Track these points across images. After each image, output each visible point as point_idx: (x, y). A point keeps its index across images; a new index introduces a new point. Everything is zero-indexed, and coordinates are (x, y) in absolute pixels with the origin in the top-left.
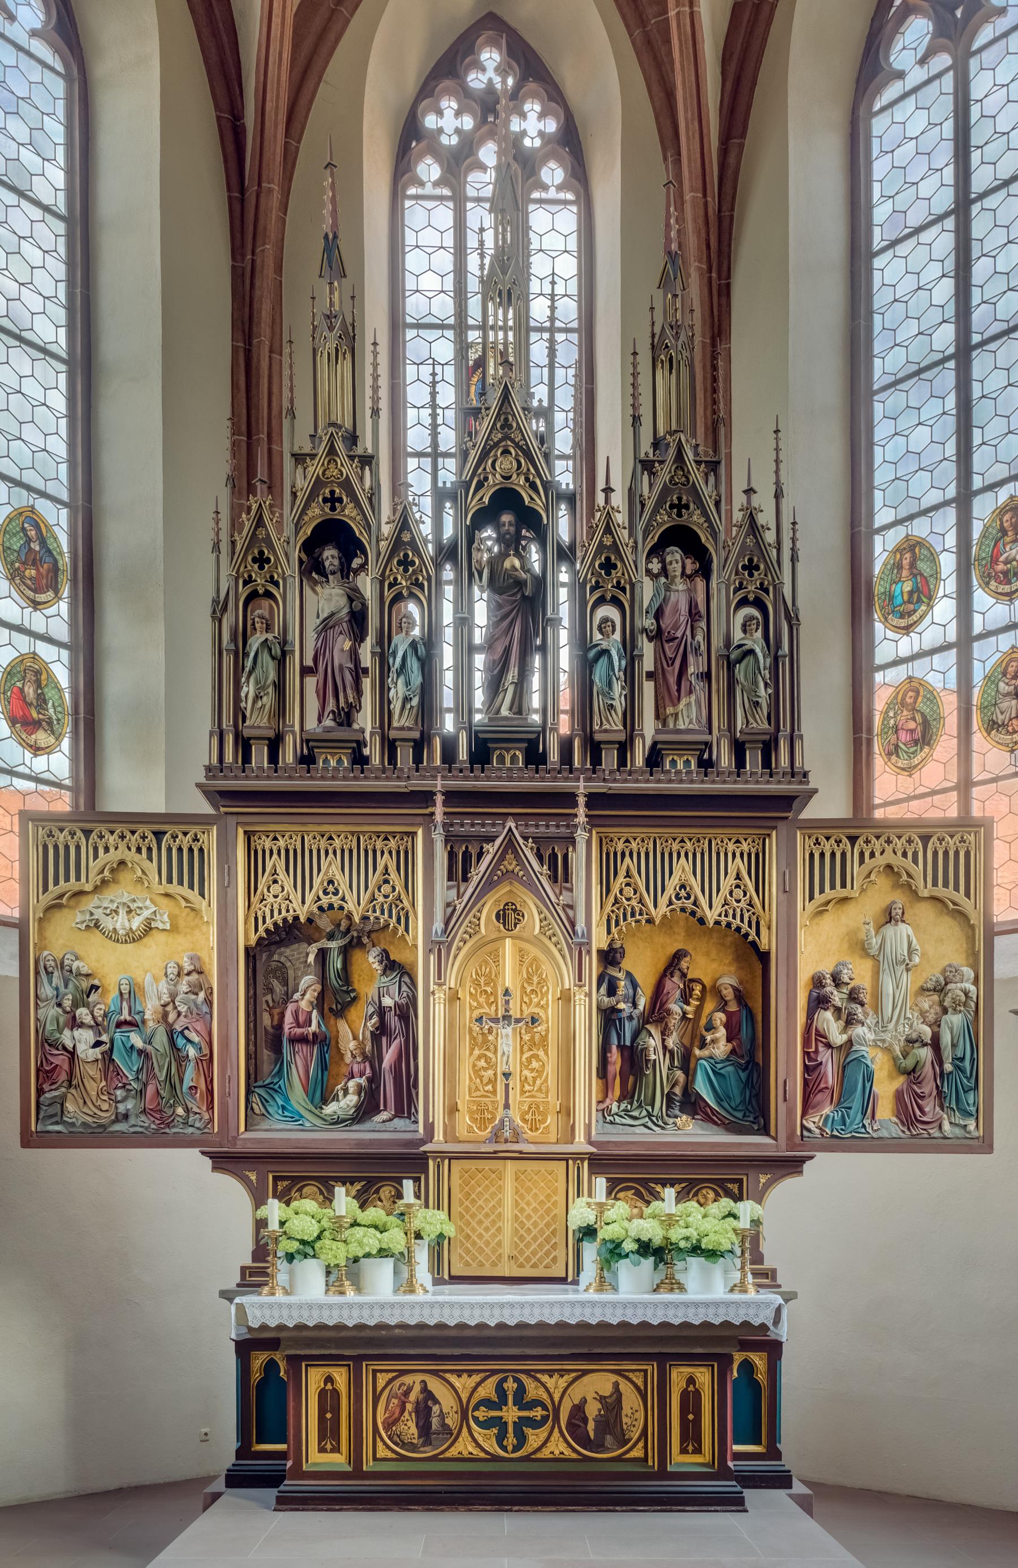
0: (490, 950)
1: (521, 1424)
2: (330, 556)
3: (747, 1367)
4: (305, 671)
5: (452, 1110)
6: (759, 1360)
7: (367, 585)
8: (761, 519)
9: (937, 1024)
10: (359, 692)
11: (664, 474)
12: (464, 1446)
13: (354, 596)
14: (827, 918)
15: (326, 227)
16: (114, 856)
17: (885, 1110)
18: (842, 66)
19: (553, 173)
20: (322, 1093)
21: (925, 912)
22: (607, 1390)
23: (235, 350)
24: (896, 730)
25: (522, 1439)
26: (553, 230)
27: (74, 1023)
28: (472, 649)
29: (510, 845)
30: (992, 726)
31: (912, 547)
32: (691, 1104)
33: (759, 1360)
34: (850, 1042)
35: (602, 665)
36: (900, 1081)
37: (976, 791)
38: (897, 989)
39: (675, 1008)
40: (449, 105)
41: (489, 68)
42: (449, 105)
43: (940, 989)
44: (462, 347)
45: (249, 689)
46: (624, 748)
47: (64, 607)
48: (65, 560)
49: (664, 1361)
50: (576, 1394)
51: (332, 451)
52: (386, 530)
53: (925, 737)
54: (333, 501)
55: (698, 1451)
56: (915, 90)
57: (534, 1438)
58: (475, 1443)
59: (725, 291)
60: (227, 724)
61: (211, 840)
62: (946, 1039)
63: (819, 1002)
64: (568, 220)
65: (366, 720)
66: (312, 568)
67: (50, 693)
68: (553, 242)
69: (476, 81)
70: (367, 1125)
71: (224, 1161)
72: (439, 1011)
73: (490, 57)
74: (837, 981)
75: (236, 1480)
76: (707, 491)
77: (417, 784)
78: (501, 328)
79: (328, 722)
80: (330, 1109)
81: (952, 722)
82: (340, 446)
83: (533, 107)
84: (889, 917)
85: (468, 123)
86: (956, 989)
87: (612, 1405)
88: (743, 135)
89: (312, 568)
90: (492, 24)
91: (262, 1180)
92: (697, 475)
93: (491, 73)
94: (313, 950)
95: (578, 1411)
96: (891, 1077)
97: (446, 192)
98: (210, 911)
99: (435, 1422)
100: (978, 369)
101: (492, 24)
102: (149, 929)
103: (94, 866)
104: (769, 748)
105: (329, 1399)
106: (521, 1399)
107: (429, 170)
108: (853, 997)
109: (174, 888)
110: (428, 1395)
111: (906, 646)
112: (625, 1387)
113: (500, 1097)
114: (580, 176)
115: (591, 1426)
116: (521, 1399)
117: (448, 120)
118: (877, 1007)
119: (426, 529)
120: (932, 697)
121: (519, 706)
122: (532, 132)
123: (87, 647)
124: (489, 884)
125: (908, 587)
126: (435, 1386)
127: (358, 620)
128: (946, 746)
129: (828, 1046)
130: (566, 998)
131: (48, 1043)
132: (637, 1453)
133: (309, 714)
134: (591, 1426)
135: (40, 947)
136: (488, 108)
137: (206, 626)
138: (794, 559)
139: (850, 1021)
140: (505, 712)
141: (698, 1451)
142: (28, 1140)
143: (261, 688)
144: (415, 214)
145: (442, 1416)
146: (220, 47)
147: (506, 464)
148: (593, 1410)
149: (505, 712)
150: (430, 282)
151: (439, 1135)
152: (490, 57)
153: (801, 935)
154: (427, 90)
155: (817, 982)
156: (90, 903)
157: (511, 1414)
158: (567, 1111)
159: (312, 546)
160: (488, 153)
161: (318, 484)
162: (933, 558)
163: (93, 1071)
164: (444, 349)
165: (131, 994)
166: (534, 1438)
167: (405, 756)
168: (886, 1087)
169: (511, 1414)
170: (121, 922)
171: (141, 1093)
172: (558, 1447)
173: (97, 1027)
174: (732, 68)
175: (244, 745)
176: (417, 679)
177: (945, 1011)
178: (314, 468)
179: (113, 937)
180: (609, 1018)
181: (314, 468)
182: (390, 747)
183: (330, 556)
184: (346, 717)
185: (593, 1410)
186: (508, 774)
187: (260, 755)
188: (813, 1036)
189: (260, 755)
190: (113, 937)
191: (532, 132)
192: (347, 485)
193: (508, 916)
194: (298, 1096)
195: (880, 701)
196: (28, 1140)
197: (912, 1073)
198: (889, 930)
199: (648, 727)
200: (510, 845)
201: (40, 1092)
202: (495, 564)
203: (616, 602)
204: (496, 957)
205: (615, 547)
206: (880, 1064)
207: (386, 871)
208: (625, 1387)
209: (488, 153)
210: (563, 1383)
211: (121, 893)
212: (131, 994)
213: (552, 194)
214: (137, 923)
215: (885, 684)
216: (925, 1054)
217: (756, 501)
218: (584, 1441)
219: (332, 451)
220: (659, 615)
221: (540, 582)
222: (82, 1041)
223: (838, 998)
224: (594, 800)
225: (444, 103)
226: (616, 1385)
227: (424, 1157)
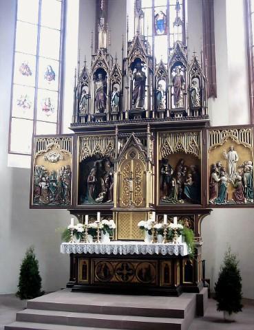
1: (128, 274)
4: (172, 95)
5: (118, 200)
8: (197, 59)
9: (242, 176)
10: (105, 104)
12: (114, 279)
14: (215, 151)
16: (52, 144)
17: (230, 198)
20: (95, 195)
21: (240, 148)
22: (147, 266)
25: (127, 278)
27: (42, 181)
32: (182, 196)
34: (221, 181)
36: (234, 190)
38: (233, 167)
39: (179, 173)
43: (244, 167)
50: (140, 267)
55: (168, 282)
57: (130, 278)
58: (116, 278)
60: (76, 114)
61: (72, 139)
62: (245, 179)
63: (213, 171)
65: (107, 111)
66: (96, 79)
70: (105, 203)
71: (72, 212)
74: (217, 166)
75: (68, 286)
76: (185, 54)
79: (97, 112)
80: (98, 199)
84: (230, 150)
86: (247, 167)
87: (148, 270)
89: (96, 79)
92: (182, 50)
94: (95, 163)
95: (140, 272)
96: (232, 189)
98: (71, 155)
99: (108, 273)
102: (58, 160)
103: (47, 146)
104: (200, 110)
105: (84, 267)
106: (128, 269)
108: (222, 170)
109: (64, 150)
110: (106, 267)
112: (152, 266)
115: (143, 276)
116: (128, 269)
118: (228, 171)
121: (141, 104)
126: (108, 264)
127: (105, 89)
129: (215, 181)
131: (36, 185)
132: (154, 282)
133: (93, 111)
134: (143, 276)
135: (36, 164)
137: (73, 93)
139: (221, 176)
140: (137, 107)
141: (168, 282)
142: (31, 207)
143: (84, 106)
145: (109, 272)
148: (144, 271)
151: (115, 206)
153: (208, 155)
155: (213, 166)
156: (46, 154)
157: (125, 272)
159: (96, 74)
163: (46, 192)
165: (55, 173)
166: (130, 278)
167: (114, 118)
168: (230, 191)
169: (125, 272)
170: (52, 158)
171: (55, 196)
172: (135, 280)
173: (47, 182)
175: (79, 118)
177: (245, 172)
178: (96, 58)
179: (51, 161)
180: (163, 176)
181: (96, 58)
182: (111, 116)
184: (102, 111)
185: (144, 271)
186: (138, 122)
187: (83, 120)
188: (212, 179)
189: (83, 120)
190: (51, 161)
192: (103, 61)
193: (132, 155)
194: (90, 197)
196: (31, 207)
197: (237, 188)
198: (230, 153)
201: (34, 196)
202: (135, 74)
203: (197, 77)
204: (130, 164)
206: (228, 185)
207: (110, 144)
210: (137, 264)
211: (52, 152)
212: (55, 173)
214: (56, 158)
216: (240, 182)
217: (196, 55)
218: (141, 278)
222: (43, 185)
223: (217, 170)
224: (151, 126)
226: (149, 266)
227: (112, 211)
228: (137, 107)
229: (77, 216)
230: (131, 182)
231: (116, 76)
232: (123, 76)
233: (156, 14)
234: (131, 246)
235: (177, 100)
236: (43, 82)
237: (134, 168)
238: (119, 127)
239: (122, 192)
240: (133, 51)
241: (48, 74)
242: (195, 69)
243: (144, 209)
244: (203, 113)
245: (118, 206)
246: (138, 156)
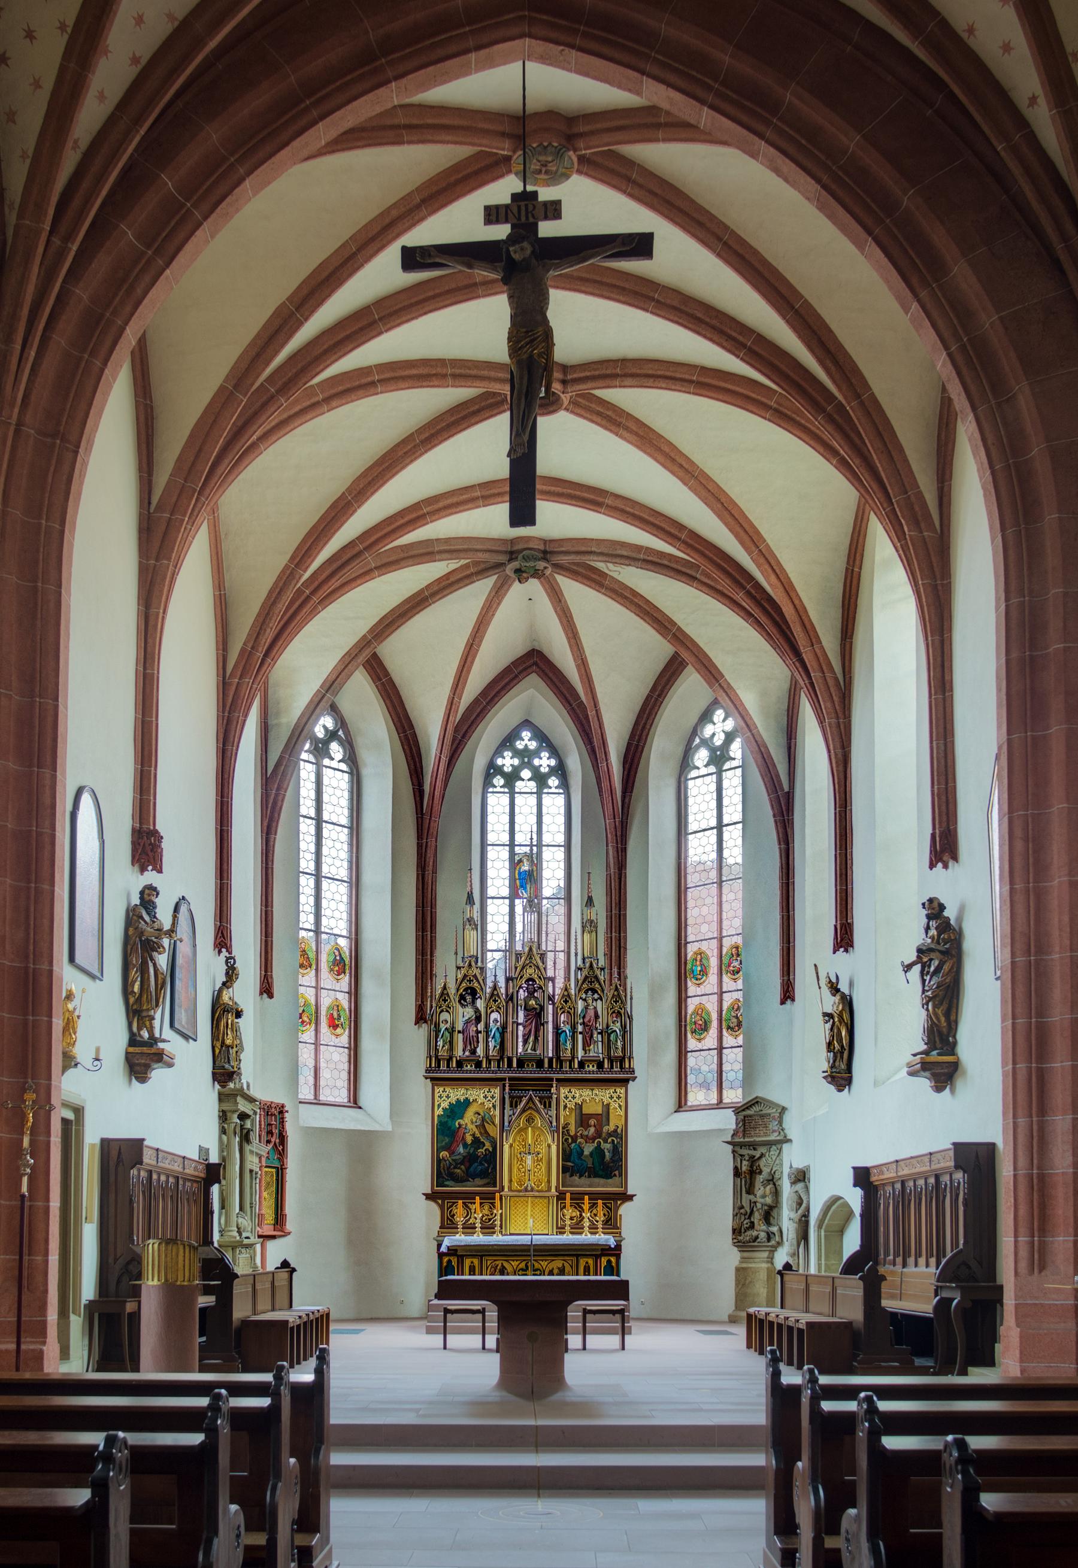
0: (524, 1130)
2: (469, 998)
3: (609, 1262)
5: (510, 1181)
6: (613, 1259)
7: (480, 1004)
11: (585, 972)
13: (477, 1011)
15: (468, 889)
18: (673, 765)
19: (553, 782)
22: (560, 1266)
23: (418, 875)
24: (695, 1023)
26: (554, 803)
28: (518, 1024)
29: (531, 1099)
30: (729, 1028)
31: (700, 953)
33: (613, 1259)
35: (563, 1035)
37: (724, 1051)
40: (508, 754)
41: (526, 740)
42: (508, 754)
44: (512, 854)
45: (440, 1043)
46: (571, 1061)
47: (347, 978)
48: (347, 961)
49: (577, 1256)
51: (470, 965)
52: (488, 990)
53: (705, 1028)
54: (470, 981)
56: (703, 776)
59: (624, 850)
60: (433, 1053)
64: (560, 800)
65: (480, 1051)
67: (342, 1013)
68: (553, 810)
69: (520, 745)
72: (506, 1147)
73: (526, 735)
77: (499, 1075)
78: (530, 331)
79: (467, 1053)
81: (715, 1024)
82: (473, 964)
83: (545, 754)
85: (516, 762)
88: (631, 792)
90: (527, 723)
91: (443, 1202)
93: (526, 741)
97: (506, 790)
100: (725, 890)
101: (527, 723)
104: (622, 1060)
107: (499, 781)
111: (699, 991)
112: (566, 1264)
113: (527, 1177)
114: (565, 784)
117: (507, 761)
119: (503, 991)
120: (708, 1014)
122: (545, 765)
123: (355, 993)
124: (523, 1111)
125: (699, 968)
126: (506, 1264)
128: (713, 1031)
130: (549, 1146)
136: (526, 756)
138: (631, 999)
144: (492, 799)
146: (415, 763)
147: (530, 971)
149: (529, 1051)
150: (499, 827)
151: (506, 1189)
152: (526, 735)
154: (498, 752)
158: (549, 1181)
160: (526, 774)
161: (465, 976)
162: (708, 959)
164: (505, 853)
167: (494, 1066)
174: (627, 766)
175: (438, 1061)
176: (499, 1040)
178: (463, 971)
181: (463, 971)
182: (489, 1061)
183: (469, 998)
184: (473, 1052)
186: (531, 1072)
187: (443, 1066)
191: (545, 765)
193: (530, 1120)
195: (691, 1009)
199: (580, 1053)
200: (531, 1099)
204: (526, 1134)
205: (569, 995)
208: (566, 1264)
209: (526, 774)
213: (553, 790)
215: (692, 1005)
219: (470, 965)
220: (584, 1017)
221: (542, 1008)
225: (505, 754)
228: (529, 1051)
229: (437, 1203)
230: (530, 1157)
231: (495, 1001)
232: (507, 1003)
233: (517, 858)
234: (43, 1325)
235: (586, 1045)
236: (327, 979)
237: (533, 1138)
238: (511, 1079)
239: (515, 1171)
240: (523, 968)
241: (335, 963)
242: (616, 1002)
243: (547, 1194)
244: (627, 1066)
245: (510, 1189)
246: (538, 1122)
